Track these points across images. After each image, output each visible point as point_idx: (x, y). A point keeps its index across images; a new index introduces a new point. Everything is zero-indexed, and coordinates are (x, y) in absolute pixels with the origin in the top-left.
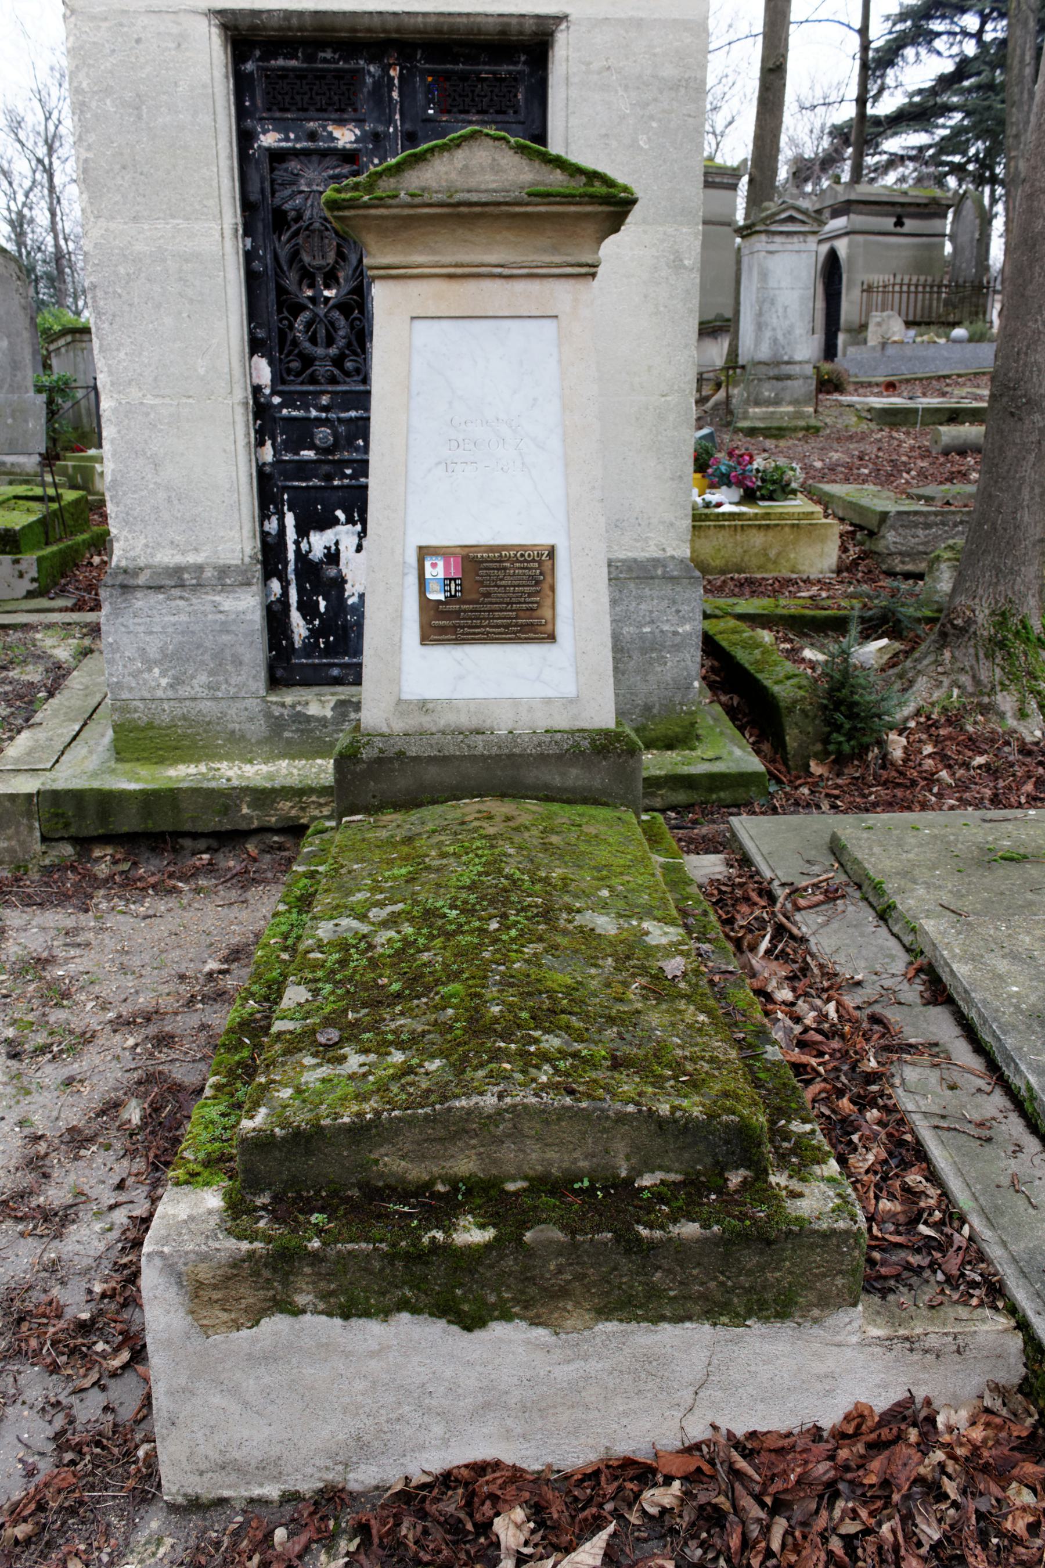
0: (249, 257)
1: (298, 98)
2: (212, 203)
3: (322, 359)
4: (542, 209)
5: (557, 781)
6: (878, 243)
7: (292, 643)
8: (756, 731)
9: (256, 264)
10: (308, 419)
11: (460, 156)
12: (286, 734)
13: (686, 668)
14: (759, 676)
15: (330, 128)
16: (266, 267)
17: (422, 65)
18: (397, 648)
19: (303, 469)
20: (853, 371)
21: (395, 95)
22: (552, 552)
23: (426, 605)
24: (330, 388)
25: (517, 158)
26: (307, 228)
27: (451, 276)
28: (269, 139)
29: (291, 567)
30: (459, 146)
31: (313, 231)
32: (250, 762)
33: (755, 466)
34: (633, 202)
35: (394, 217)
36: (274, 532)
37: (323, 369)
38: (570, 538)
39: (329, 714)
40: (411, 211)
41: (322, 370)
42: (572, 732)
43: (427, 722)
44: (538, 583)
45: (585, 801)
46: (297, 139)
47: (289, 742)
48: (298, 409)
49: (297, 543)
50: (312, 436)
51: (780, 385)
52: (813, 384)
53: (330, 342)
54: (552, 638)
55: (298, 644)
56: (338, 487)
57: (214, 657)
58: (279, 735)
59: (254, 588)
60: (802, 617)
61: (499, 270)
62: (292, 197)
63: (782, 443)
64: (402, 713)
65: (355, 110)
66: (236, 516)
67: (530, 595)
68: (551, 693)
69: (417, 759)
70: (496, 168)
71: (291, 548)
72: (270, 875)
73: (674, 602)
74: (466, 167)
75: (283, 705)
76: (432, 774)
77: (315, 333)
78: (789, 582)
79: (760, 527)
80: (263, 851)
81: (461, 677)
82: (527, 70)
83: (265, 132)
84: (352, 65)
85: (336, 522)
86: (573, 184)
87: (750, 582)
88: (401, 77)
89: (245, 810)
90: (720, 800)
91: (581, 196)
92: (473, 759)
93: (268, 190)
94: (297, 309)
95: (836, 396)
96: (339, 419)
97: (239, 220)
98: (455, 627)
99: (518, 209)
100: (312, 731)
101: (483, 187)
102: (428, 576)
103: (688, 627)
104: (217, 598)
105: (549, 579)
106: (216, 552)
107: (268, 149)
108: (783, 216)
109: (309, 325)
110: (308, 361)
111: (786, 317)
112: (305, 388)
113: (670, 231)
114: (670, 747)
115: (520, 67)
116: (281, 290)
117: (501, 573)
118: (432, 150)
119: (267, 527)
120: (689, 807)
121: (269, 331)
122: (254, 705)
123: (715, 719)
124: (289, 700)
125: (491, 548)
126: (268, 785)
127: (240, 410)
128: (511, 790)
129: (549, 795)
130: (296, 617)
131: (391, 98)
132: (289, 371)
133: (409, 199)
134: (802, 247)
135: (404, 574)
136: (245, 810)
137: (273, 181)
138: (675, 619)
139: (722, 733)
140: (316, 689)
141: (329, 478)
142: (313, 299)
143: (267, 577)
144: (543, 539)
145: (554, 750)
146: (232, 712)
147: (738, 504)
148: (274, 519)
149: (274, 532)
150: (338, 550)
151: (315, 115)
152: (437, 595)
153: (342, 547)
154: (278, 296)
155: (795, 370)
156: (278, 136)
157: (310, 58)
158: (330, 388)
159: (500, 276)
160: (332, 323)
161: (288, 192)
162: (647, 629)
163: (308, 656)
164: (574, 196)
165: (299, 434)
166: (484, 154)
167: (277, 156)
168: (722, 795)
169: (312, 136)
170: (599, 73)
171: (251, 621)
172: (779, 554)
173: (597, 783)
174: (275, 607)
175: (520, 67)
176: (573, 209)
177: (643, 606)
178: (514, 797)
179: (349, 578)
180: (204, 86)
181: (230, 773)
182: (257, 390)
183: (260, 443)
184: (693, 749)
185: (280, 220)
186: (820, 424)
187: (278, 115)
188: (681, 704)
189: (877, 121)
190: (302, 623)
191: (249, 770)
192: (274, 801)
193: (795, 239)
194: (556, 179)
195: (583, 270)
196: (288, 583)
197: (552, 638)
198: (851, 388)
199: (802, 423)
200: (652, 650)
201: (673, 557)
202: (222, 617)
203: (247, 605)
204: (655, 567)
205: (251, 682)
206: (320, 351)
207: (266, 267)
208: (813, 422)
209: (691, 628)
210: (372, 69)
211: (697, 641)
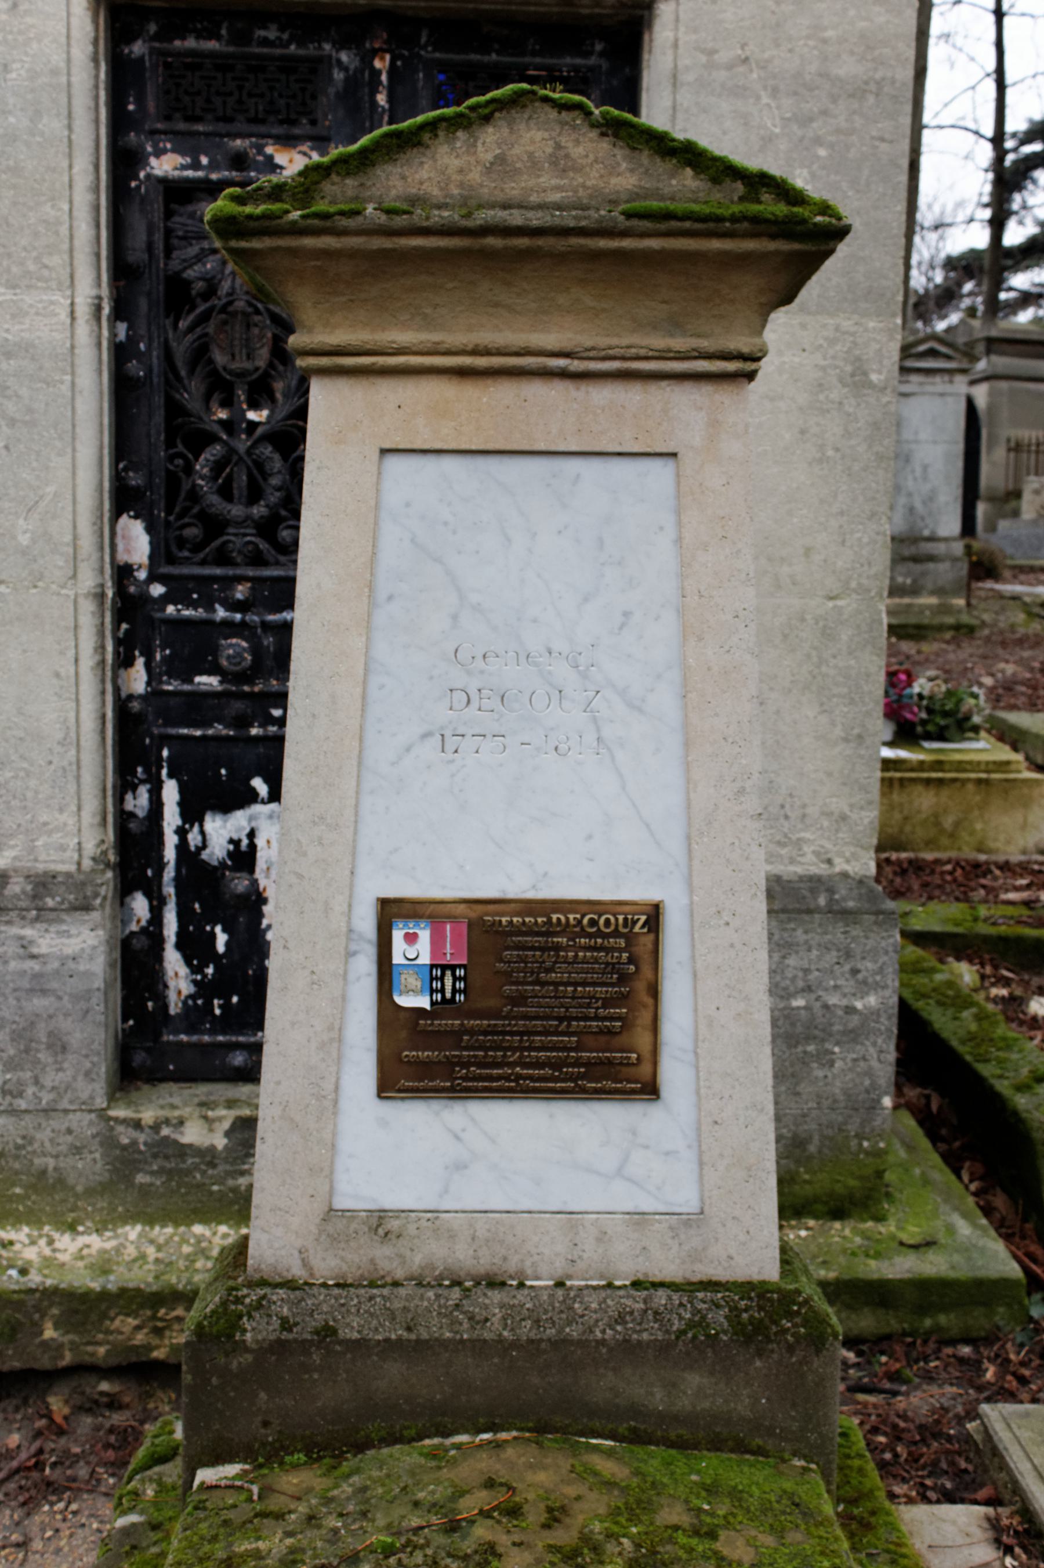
0: (121, 353)
1: (218, 101)
2: (57, 261)
3: (240, 524)
4: (654, 243)
5: (658, 1399)
6: (1028, 392)
7: (163, 1005)
8: (979, 1168)
9: (134, 367)
10: (210, 623)
11: (490, 140)
12: (141, 1178)
13: (869, 1073)
14: (986, 1070)
15: (269, 150)
16: (149, 371)
17: (428, 53)
18: (329, 1102)
19: (198, 708)
20: (1009, 550)
21: (382, 99)
22: (654, 915)
23: (389, 1016)
24: (250, 572)
25: (605, 145)
26: (224, 310)
27: (463, 373)
28: (166, 165)
29: (169, 873)
30: (487, 119)
31: (234, 314)
32: (72, 1228)
33: (916, 689)
34: (841, 232)
35: (353, 254)
36: (141, 813)
37: (239, 540)
38: (691, 889)
39: (220, 1142)
40: (387, 243)
41: (239, 542)
42: (689, 1287)
43: (386, 1258)
44: (624, 978)
45: (716, 1445)
46: (213, 166)
47: (145, 1192)
48: (194, 605)
49: (181, 832)
50: (215, 650)
51: (918, 568)
52: (964, 569)
53: (254, 495)
54: (651, 1090)
55: (174, 1007)
56: (257, 739)
57: (16, 1036)
58: (128, 1179)
59: (96, 915)
60: (1019, 940)
61: (562, 362)
62: (200, 258)
63: (926, 647)
64: (334, 1239)
65: (313, 123)
66: (72, 788)
67: (607, 1003)
68: (647, 1204)
69: (360, 1345)
70: (561, 163)
71: (171, 841)
72: (83, 1472)
73: (848, 955)
74: (500, 159)
75: (137, 1125)
76: (391, 1377)
77: (229, 479)
78: (978, 870)
79: (928, 782)
80: (80, 1409)
81: (460, 1166)
82: (605, 65)
83: (159, 153)
84: (311, 50)
85: (252, 797)
86: (717, 195)
87: (917, 866)
88: (392, 71)
89: (49, 1333)
90: (937, 1329)
91: (734, 219)
92: (479, 1347)
93: (160, 245)
94: (201, 440)
95: (989, 584)
96: (265, 626)
97: (105, 292)
98: (450, 1064)
99: (603, 243)
100: (188, 1172)
101: (534, 198)
102: (397, 959)
103: (872, 1000)
104: (28, 932)
105: (647, 972)
106: (32, 850)
107: (164, 182)
108: (922, 348)
109: (218, 467)
110: (215, 526)
111: (925, 478)
112: (207, 571)
113: (847, 325)
114: (838, 1214)
115: (593, 61)
116: (174, 410)
117: (549, 958)
118: (432, 126)
119: (130, 804)
120: (881, 1342)
121: (151, 474)
122: (84, 1124)
123: (910, 1148)
124: (148, 1115)
125: (530, 906)
126: (95, 1285)
127: (88, 607)
128: (555, 1420)
129: (638, 1431)
130: (173, 960)
131: (374, 103)
132: (181, 543)
133: (383, 218)
134: (948, 388)
135: (350, 954)
136: (49, 1333)
137: (168, 233)
138: (848, 985)
139: (926, 1181)
140: (202, 1090)
141: (242, 722)
142: (228, 426)
143: (124, 891)
144: (636, 891)
145: (650, 1333)
146: (44, 1136)
147: (891, 744)
148: (143, 792)
149: (141, 813)
150: (253, 847)
151: (245, 127)
152: (414, 999)
153: (260, 842)
154: (169, 419)
155: (940, 548)
156: (180, 160)
157: (240, 38)
158: (250, 572)
159: (564, 374)
160: (259, 465)
161: (193, 250)
162: (799, 1002)
163: (191, 1030)
164: (719, 219)
165: (195, 647)
166: (539, 135)
167: (178, 193)
168: (943, 1319)
169: (239, 161)
170: (730, 67)
171: (88, 974)
172: (957, 824)
173: (742, 1407)
174: (137, 944)
175: (593, 61)
176: (716, 244)
177: (792, 961)
178: (564, 1430)
179: (270, 894)
180: (54, 72)
181: (30, 1254)
182: (123, 573)
183: (124, 661)
184: (880, 1218)
185: (178, 296)
186: (974, 622)
187: (182, 126)
188: (860, 1137)
189: (1010, 252)
190: (183, 970)
191: (67, 1245)
192: (104, 1316)
193: (938, 379)
194: (685, 186)
195: (731, 366)
196: (162, 901)
197: (651, 1090)
198: (1007, 574)
199: (950, 620)
200: (809, 1038)
201: (845, 875)
202: (35, 966)
203: (82, 946)
204: (814, 892)
205: (81, 1083)
206: (237, 511)
207: (149, 371)
208: (965, 619)
209: (878, 1002)
210: (344, 57)
211: (889, 1024)
